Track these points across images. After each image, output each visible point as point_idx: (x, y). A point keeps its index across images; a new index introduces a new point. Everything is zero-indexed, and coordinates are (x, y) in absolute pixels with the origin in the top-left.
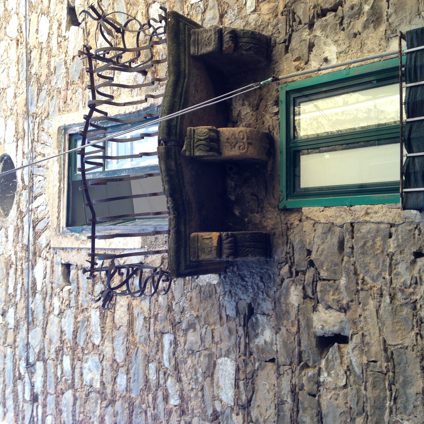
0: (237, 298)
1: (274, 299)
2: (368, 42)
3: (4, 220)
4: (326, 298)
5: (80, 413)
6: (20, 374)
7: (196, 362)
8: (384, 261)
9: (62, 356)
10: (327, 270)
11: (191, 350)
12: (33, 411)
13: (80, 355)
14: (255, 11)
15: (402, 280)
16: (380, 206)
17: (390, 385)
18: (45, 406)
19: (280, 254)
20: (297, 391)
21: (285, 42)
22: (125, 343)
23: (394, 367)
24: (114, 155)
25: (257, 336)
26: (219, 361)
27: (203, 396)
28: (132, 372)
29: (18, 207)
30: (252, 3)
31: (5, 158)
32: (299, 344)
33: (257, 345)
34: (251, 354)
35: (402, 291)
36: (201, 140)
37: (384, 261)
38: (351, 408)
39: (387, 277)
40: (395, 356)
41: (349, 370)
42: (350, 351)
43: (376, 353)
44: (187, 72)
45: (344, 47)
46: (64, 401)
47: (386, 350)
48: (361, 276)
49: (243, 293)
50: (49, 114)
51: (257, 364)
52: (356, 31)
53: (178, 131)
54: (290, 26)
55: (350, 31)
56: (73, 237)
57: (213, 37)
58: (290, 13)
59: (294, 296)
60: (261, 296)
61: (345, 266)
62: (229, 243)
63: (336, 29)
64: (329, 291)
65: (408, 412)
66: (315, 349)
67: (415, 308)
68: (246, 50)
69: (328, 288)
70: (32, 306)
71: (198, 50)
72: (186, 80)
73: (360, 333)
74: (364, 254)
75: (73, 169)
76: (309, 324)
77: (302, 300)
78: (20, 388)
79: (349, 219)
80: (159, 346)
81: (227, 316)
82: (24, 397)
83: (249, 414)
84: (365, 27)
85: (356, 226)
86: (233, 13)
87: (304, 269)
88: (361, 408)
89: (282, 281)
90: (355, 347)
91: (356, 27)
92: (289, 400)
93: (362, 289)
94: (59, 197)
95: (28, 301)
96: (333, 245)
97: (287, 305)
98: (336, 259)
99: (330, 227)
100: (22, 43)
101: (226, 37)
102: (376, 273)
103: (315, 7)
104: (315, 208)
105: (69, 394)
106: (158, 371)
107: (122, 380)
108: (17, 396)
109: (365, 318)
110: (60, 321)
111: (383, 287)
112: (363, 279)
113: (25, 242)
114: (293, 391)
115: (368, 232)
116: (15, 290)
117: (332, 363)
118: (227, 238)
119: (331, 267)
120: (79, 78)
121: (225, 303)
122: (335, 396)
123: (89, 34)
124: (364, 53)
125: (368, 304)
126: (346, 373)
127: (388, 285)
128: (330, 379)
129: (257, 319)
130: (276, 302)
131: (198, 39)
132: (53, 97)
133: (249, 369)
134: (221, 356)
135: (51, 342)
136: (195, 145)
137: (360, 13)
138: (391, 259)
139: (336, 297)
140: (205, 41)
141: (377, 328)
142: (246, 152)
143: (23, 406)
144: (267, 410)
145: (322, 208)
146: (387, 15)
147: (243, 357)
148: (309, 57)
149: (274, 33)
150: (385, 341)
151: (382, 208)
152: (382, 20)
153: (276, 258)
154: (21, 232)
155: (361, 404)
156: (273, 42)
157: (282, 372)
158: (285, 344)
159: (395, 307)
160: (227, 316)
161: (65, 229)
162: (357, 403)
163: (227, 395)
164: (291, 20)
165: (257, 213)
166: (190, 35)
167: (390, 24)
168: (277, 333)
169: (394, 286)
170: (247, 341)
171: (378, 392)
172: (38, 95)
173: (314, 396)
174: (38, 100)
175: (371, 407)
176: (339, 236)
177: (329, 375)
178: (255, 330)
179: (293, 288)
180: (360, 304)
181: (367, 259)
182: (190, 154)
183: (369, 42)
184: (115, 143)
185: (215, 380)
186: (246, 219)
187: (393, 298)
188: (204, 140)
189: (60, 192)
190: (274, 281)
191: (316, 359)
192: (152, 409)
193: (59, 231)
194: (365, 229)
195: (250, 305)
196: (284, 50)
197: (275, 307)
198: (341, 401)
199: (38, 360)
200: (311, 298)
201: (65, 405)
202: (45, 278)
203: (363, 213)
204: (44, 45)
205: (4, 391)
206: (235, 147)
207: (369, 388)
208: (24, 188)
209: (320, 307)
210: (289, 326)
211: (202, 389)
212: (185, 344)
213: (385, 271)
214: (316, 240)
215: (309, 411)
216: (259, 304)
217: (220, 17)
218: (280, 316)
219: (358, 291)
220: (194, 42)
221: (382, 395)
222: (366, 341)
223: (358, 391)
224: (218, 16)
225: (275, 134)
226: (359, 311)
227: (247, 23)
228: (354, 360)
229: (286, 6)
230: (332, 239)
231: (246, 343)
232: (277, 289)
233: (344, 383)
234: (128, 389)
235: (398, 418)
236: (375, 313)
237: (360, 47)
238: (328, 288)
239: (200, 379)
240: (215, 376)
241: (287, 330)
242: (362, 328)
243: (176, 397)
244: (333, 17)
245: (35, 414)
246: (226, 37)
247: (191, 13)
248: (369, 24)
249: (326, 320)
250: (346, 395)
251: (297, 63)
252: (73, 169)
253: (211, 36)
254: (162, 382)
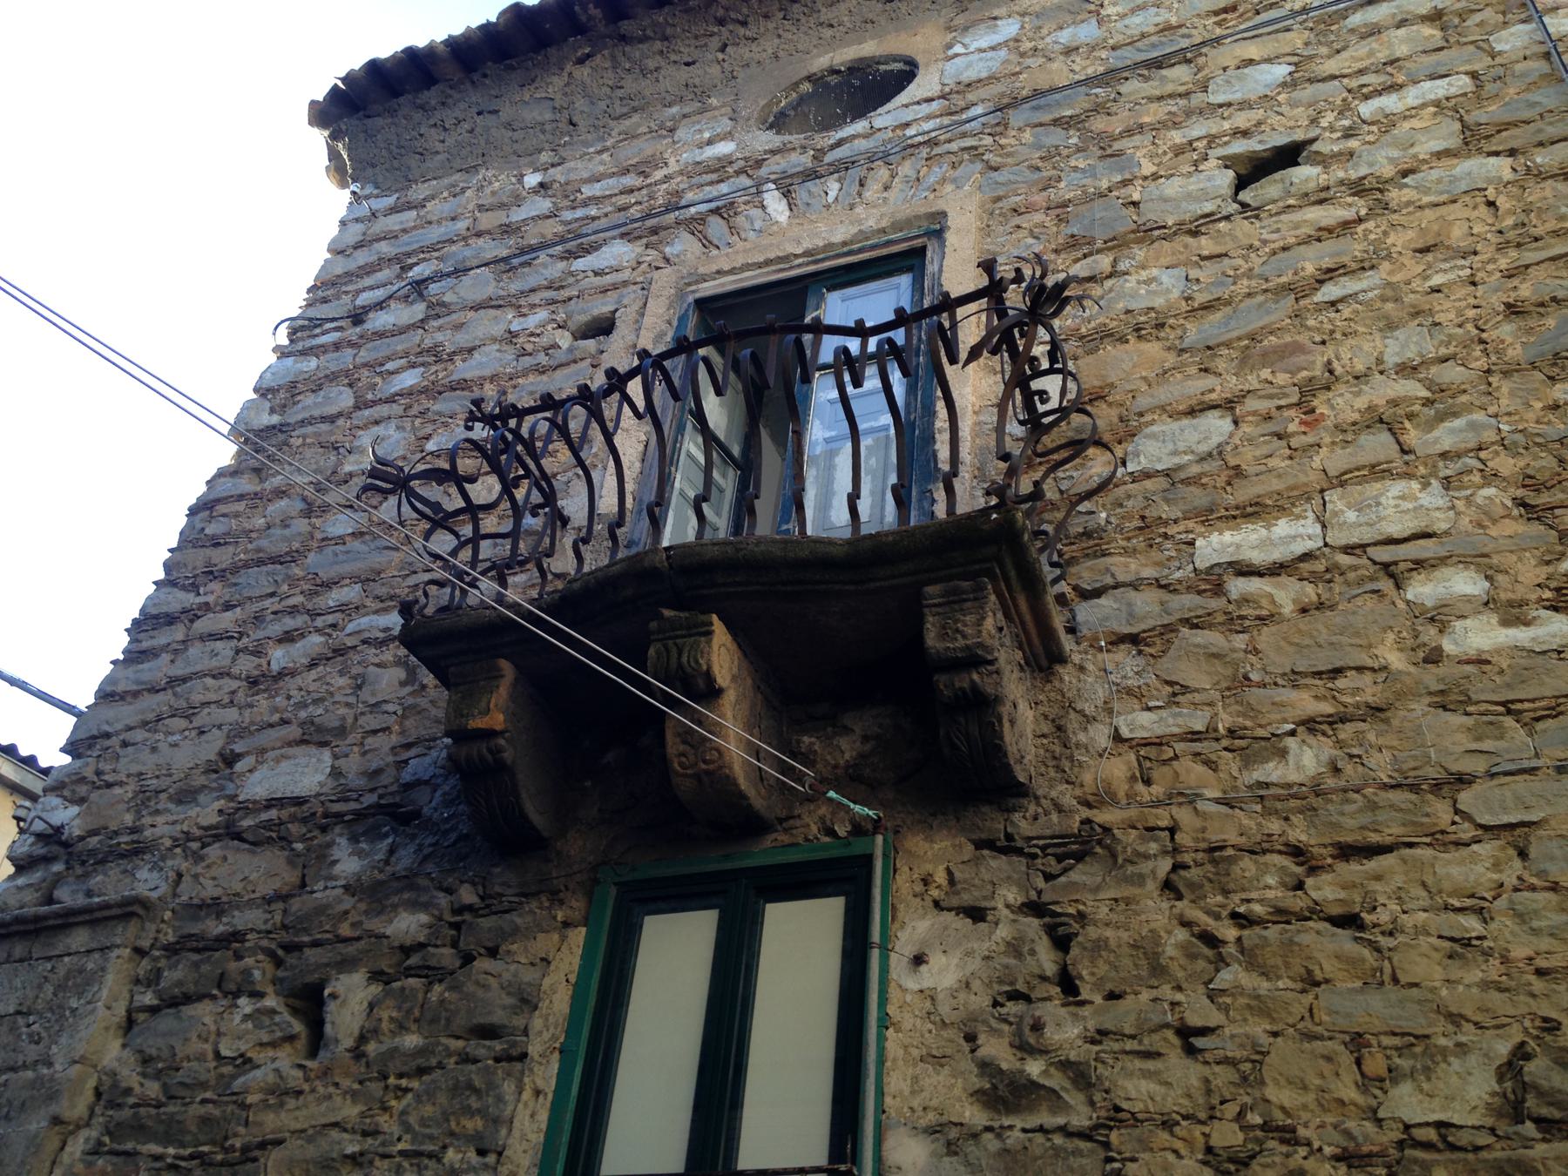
1: (416, 875)
3: (752, 122)
5: (304, 437)
6: (411, 267)
7: (338, 698)
10: (442, 1002)
11: (363, 683)
13: (415, 410)
14: (1117, 738)
16: (544, 1126)
18: (337, 346)
19: (504, 879)
21: (1009, 837)
23: (232, 1165)
25: (354, 839)
30: (1142, 727)
32: (316, 944)
37: (431, 1138)
38: (178, 1070)
39: (400, 1146)
42: (277, 1064)
43: (260, 1124)
45: (945, 1009)
48: (415, 1084)
50: (996, 169)
51: (299, 846)
52: (982, 1039)
53: (705, 592)
54: (1043, 848)
55: (985, 1022)
56: (664, 326)
57: (961, 643)
58: (1081, 843)
59: (407, 924)
61: (439, 1043)
63: (1001, 982)
69: (406, 1006)
70: (543, 257)
71: (935, 605)
72: (851, 588)
73: (306, 1087)
75: (838, 281)
76: (346, 965)
77: (396, 944)
78: (385, 274)
79: (534, 1049)
83: (217, 838)
84: (986, 1067)
85: (518, 1066)
86: (1131, 674)
87: (461, 944)
89: (449, 891)
90: (281, 1077)
91: (993, 1040)
93: (387, 1087)
94: (768, 262)
95: (555, 244)
96: (489, 1013)
98: (460, 1022)
100: (1219, 24)
101: (962, 681)
103: (1081, 916)
104: (576, 961)
106: (342, 608)
108: (368, 274)
109: (330, 1097)
110: (494, 340)
111: (381, 1138)
112: (406, 1090)
113: (690, 196)
114: (237, 936)
116: (585, 204)
118: (490, 750)
119: (446, 1010)
120: (1073, 236)
122: (204, 1035)
123: (1195, 233)
125: (354, 1102)
128: (237, 1019)
130: (408, 880)
131: (965, 600)
132: (1038, 169)
133: (294, 828)
134: (335, 757)
135: (459, 327)
136: (670, 642)
137: (1025, 1049)
138: (431, 1156)
139: (385, 1025)
140: (957, 621)
141: (305, 1126)
143: (346, 293)
144: (214, 879)
145: (573, 978)
146: (1001, 1127)
148: (949, 910)
149: (1038, 804)
152: (999, 1112)
154: (714, 177)
156: (1013, 801)
159: (338, 1165)
161: (691, 299)
164: (1059, 850)
166: (972, 576)
167: (975, 1136)
168: (346, 888)
169: (378, 1163)
171: (193, 1129)
172: (1056, 122)
173: (219, 987)
174: (1041, 125)
175: (173, 1114)
176: (505, 1027)
177: (246, 1017)
178: (364, 834)
179: (424, 918)
180: (361, 1083)
181: (442, 1099)
186: (588, 784)
188: (680, 666)
189: (780, 260)
193: (689, 284)
194: (508, 1087)
196: (983, 836)
197: (398, 879)
198: (196, 1046)
199: (430, 306)
202: (596, 274)
203: (540, 1084)
204: (1198, 99)
205: (385, 238)
207: (202, 1110)
208: (819, 154)
209: (376, 989)
210: (354, 917)
212: (378, 665)
213: (413, 1143)
216: (413, 837)
217: (1130, 634)
218: (375, 893)
219: (386, 1078)
221: (188, 1138)
222: (287, 1099)
223: (204, 1086)
224: (1134, 630)
225: (774, 835)
226: (346, 1083)
227: (1089, 720)
228: (258, 1073)
229: (1107, 830)
232: (433, 879)
236: (333, 1120)
237: (934, 1052)
238: (406, 1006)
242: (313, 1091)
244: (1037, 971)
246: (962, 681)
248: (992, 1076)
249: (351, 1000)
250: (201, 1058)
251: (940, 877)
252: (838, 281)
253: (964, 637)
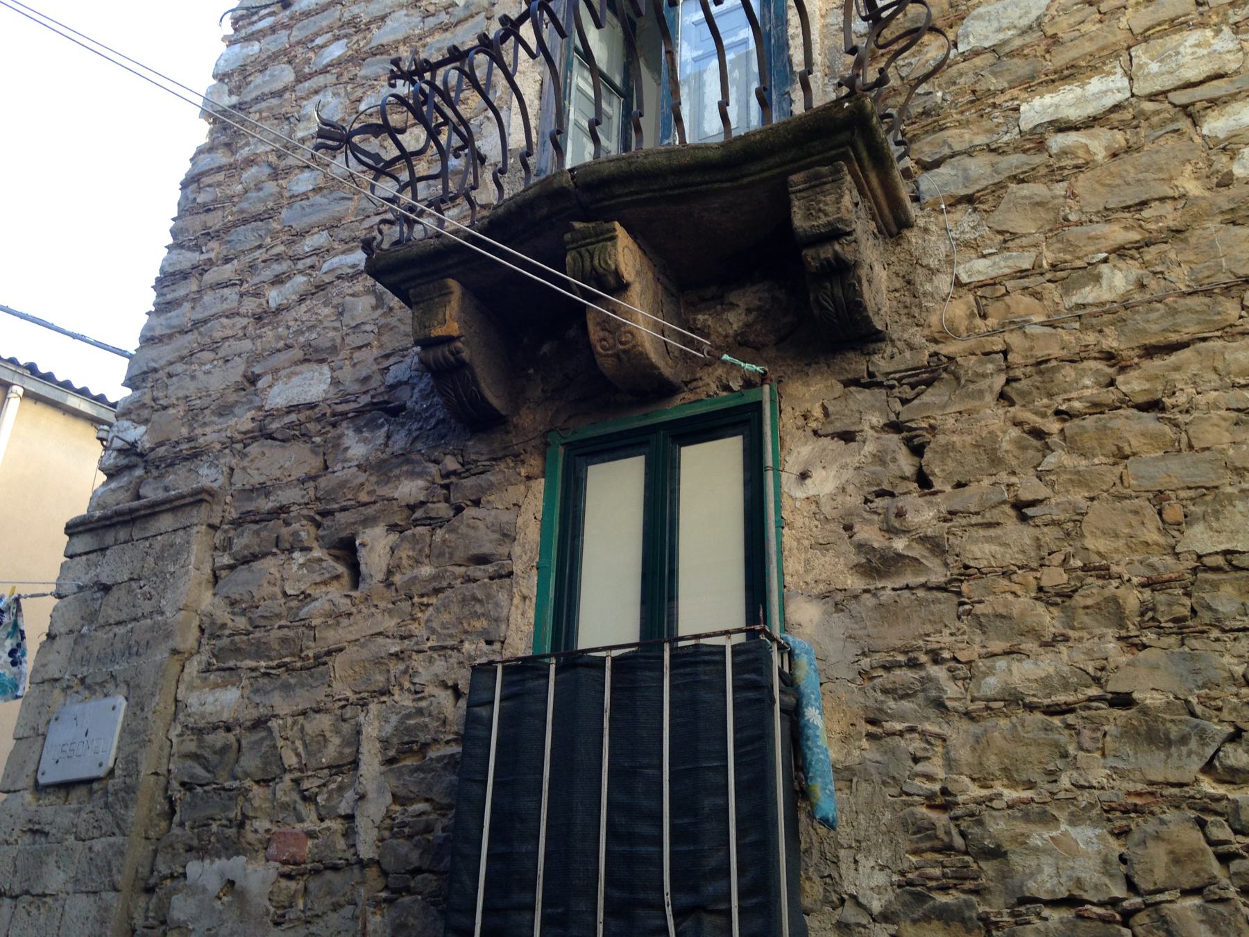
1: (410, 452)
2: (829, 558)
4: (406, 545)
7: (326, 324)
8: (451, 636)
9: (346, 36)
11: (344, 310)
12: (266, 6)
15: (420, 670)
16: (532, 621)
17: (285, 665)
20: (283, 516)
23: (309, 669)
25: (358, 430)
26: (325, 369)
27: (279, 351)
28: (318, 199)
30: (979, 272)
32: (343, 509)
33: (343, 434)
34: (334, 425)
35: (405, 672)
36: (592, 258)
37: (451, 636)
38: (257, 607)
40: (322, 668)
41: (306, 597)
42: (330, 597)
43: (325, 639)
44: (745, 181)
47: (329, 653)
48: (433, 600)
51: (318, 439)
52: (857, 528)
54: (899, 380)
55: (859, 515)
59: (409, 489)
61: (446, 571)
62: (445, 357)
63: (869, 484)
64: (414, 550)
65: (252, 695)
66: (336, 537)
67: (383, 693)
68: (817, 299)
71: (800, 191)
73: (354, 610)
74: (464, 601)
76: (368, 522)
77: (403, 504)
79: (518, 568)
83: (254, 439)
84: (861, 547)
85: (507, 581)
88: (257, 623)
89: (436, 462)
91: (866, 528)
92: (270, 505)
97: (398, 477)
98: (460, 555)
99: (507, 536)
102: (435, 625)
103: (932, 428)
105: (286, 75)
106: (316, 252)
111: (414, 640)
112: (428, 605)
115: (497, 605)
117: (317, 568)
121: (408, 360)
124: (806, 552)
126: (303, 593)
127: (415, 648)
128: (295, 567)
129: (382, 425)
130: (404, 457)
131: (825, 183)
133: (312, 427)
134: (332, 370)
136: (583, 250)
137: (891, 531)
138: (452, 648)
139: (405, 562)
142: (599, 353)
145: (539, 516)
147: (329, 411)
148: (826, 436)
149: (894, 346)
150: (341, 650)
151: (529, 624)
153: (470, 443)
155: (263, 622)
157: (306, 485)
158: (342, 485)
160: (387, 368)
162: (262, 617)
163: (279, 395)
164: (912, 380)
165: (543, 391)
167: (856, 597)
169: (415, 656)
176: (493, 555)
177: (302, 566)
178: (365, 426)
179: (421, 483)
181: (455, 608)
182: (568, 243)
183: (827, 559)
185: (298, 368)
187: (397, 656)
188: (593, 268)
190: (435, 447)
191: (326, 540)
192: (265, 257)
194: (502, 597)
195: (402, 408)
197: (397, 456)
198: (267, 590)
200: (413, 516)
201: (272, 76)
206: (603, 330)
207: (281, 633)
209: (394, 537)
211: (288, 347)
212: (352, 295)
214: (493, 512)
215: (256, 540)
218: (381, 468)
219: (411, 598)
220: (818, 176)
222: (340, 619)
223: (279, 616)
227: (933, 272)
228: (317, 604)
229: (951, 359)
230: (491, 542)
233: (289, 592)
235: (245, 682)
236: (378, 631)
239: (302, 339)
240: (305, 367)
241: (362, 484)
242: (360, 612)
244: (899, 474)
245: (263, 12)
247: (997, 113)
248: (866, 553)
249: (377, 547)
250: (273, 597)
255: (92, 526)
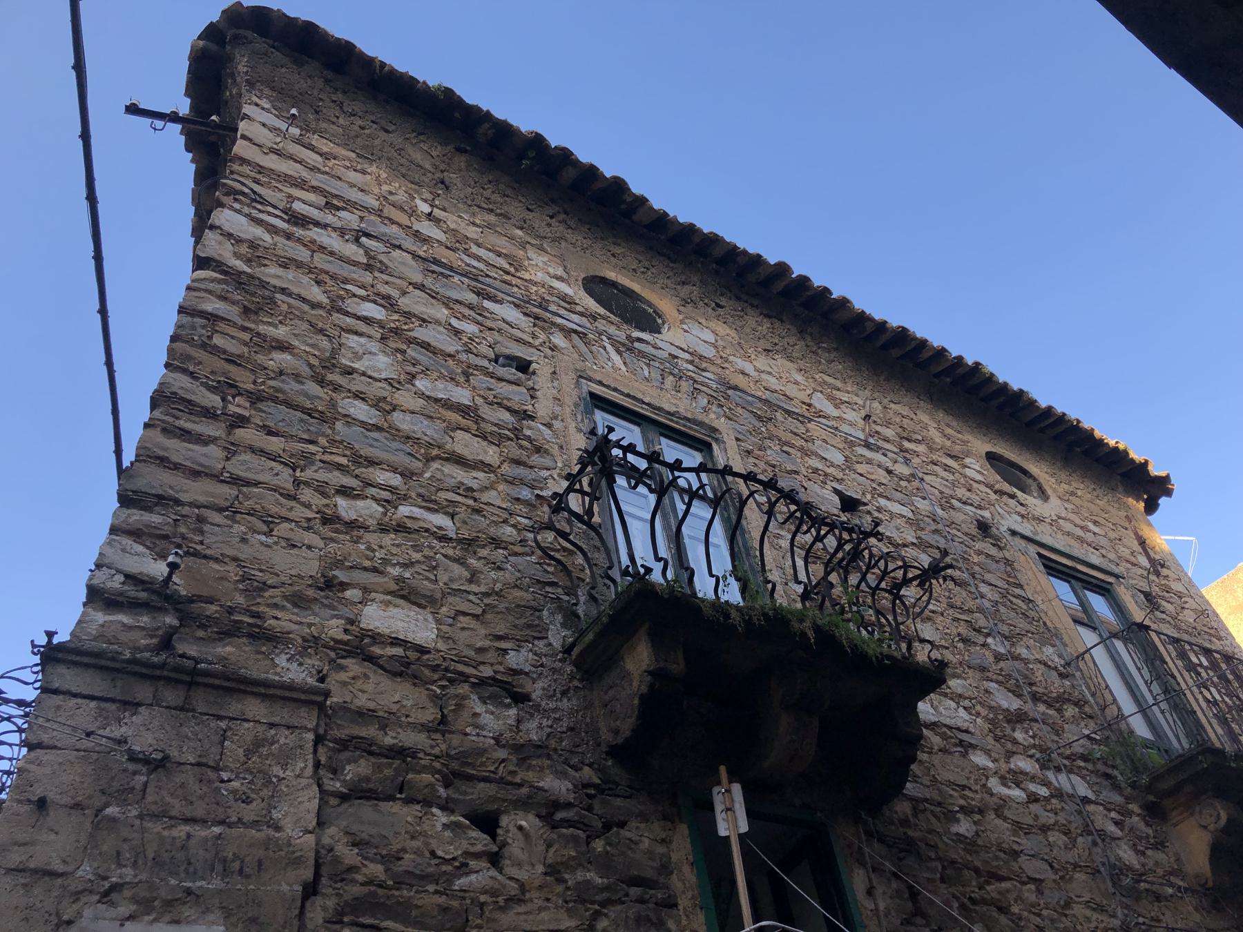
0: (535, 676)
22: (426, 438)
24: (692, 510)
29: (603, 318)
31: (660, 321)
46: (305, 279)
49: (543, 689)
60: (545, 722)
78: (311, 197)
80: (432, 505)
81: (505, 651)
82: (299, 199)
92: (388, 741)
94: (628, 396)
105: (316, 294)
107: (360, 410)
160: (505, 651)
170: (472, 680)
178: (489, 698)
184: (709, 516)
208: (629, 337)
231: (468, 677)
234: (349, 420)
243: (353, 516)
245: (270, 209)
254: (373, 491)
255: (103, 662)
